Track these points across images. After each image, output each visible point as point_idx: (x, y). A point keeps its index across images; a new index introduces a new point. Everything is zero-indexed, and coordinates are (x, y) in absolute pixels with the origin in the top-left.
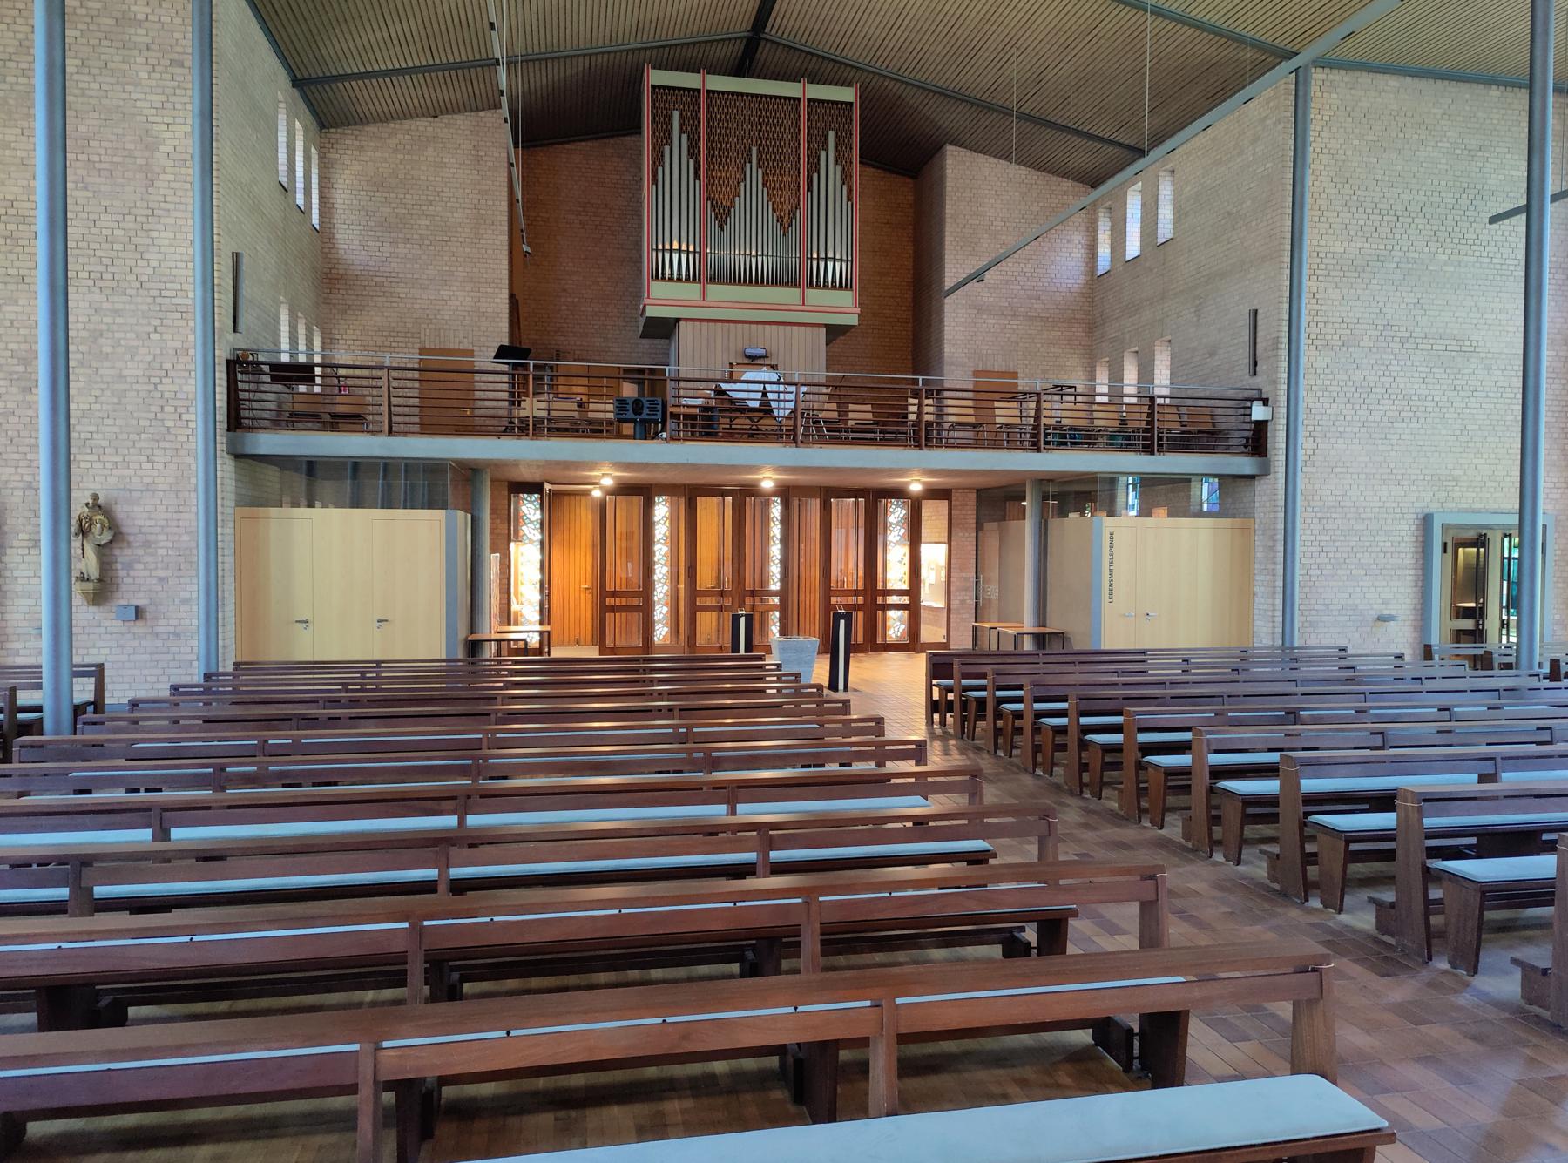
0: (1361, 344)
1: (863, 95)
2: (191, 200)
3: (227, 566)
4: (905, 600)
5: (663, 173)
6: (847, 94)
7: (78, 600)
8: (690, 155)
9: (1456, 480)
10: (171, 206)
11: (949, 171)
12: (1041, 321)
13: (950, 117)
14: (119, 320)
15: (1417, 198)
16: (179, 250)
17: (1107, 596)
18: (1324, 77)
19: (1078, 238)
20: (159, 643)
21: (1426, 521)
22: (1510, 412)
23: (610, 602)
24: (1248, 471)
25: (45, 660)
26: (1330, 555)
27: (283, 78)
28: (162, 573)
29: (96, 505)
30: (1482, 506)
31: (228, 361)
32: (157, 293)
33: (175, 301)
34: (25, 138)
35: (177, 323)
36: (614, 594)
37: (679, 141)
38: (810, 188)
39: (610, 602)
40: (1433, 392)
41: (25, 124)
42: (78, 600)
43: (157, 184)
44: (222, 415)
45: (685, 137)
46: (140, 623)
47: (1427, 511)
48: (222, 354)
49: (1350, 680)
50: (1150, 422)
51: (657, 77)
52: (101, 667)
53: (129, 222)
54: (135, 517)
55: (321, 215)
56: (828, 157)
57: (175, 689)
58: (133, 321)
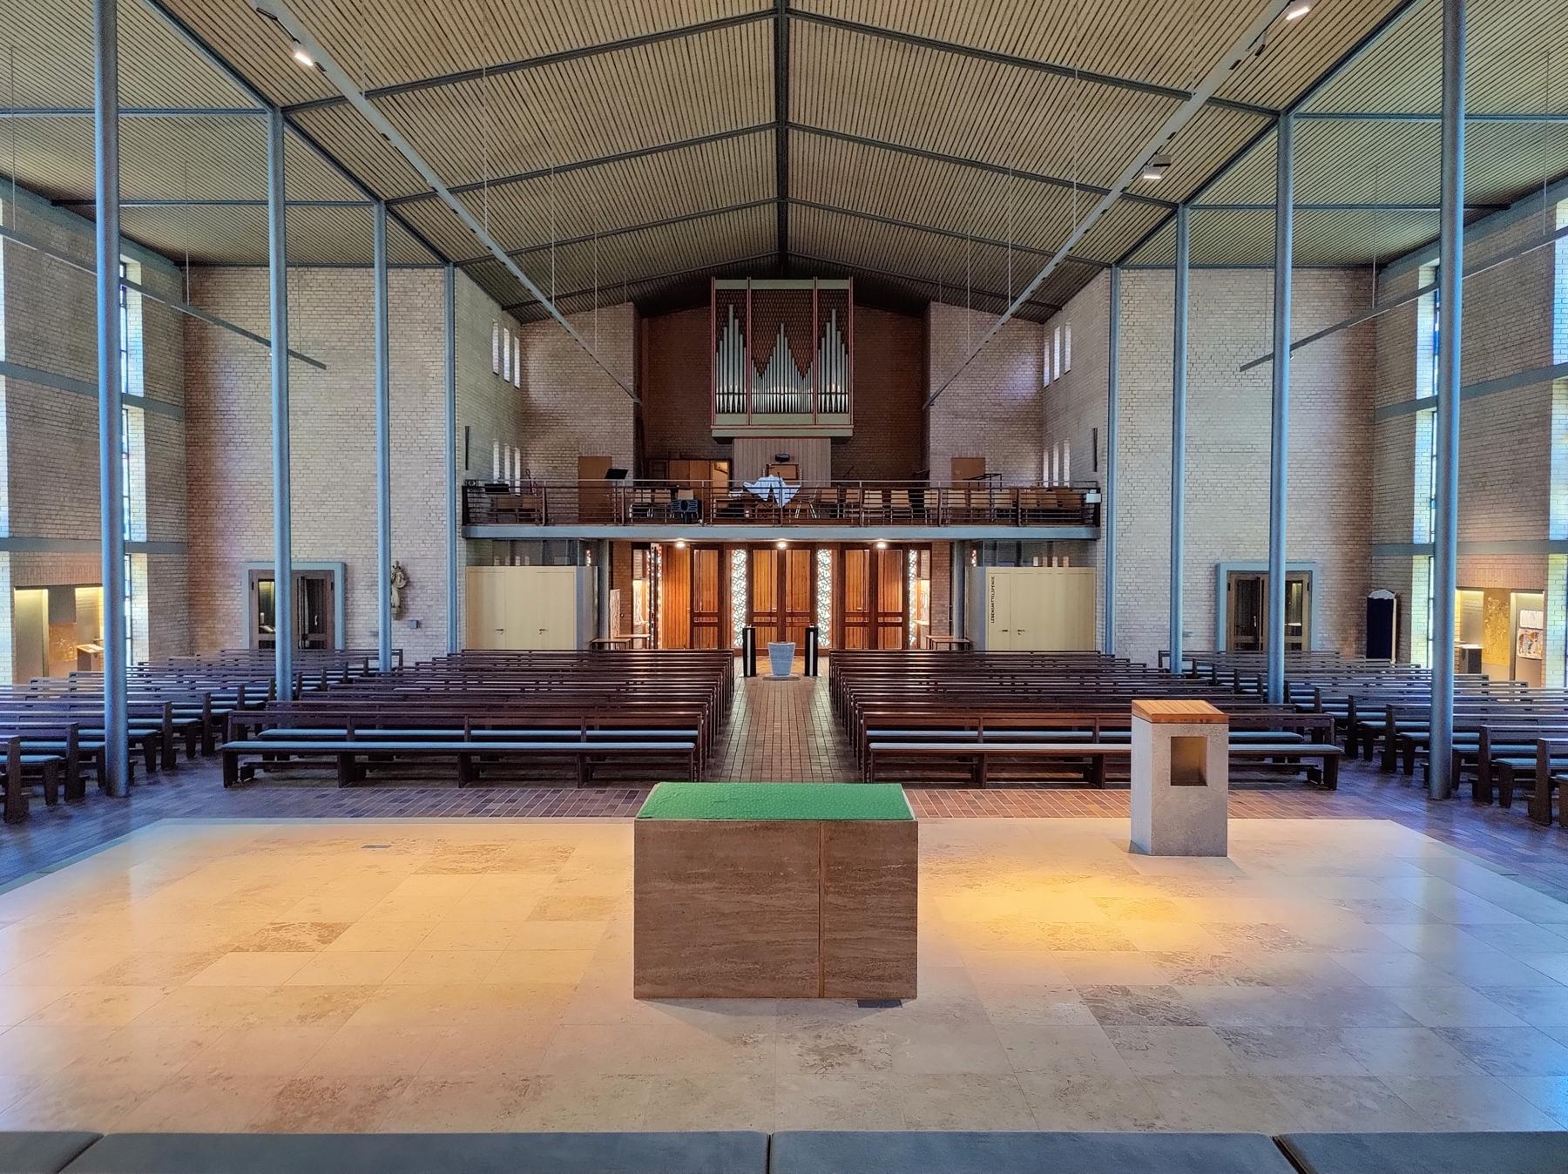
1: (856, 286)
5: (723, 345)
11: (932, 320)
18: (1135, 275)
19: (1030, 360)
21: (1217, 568)
25: (380, 647)
27: (496, 308)
36: (700, 615)
37: (733, 323)
38: (820, 348)
39: (900, 620)
44: (459, 517)
45: (737, 321)
46: (419, 630)
47: (1218, 562)
48: (460, 484)
49: (1528, 710)
50: (1016, 504)
54: (417, 572)
56: (831, 328)
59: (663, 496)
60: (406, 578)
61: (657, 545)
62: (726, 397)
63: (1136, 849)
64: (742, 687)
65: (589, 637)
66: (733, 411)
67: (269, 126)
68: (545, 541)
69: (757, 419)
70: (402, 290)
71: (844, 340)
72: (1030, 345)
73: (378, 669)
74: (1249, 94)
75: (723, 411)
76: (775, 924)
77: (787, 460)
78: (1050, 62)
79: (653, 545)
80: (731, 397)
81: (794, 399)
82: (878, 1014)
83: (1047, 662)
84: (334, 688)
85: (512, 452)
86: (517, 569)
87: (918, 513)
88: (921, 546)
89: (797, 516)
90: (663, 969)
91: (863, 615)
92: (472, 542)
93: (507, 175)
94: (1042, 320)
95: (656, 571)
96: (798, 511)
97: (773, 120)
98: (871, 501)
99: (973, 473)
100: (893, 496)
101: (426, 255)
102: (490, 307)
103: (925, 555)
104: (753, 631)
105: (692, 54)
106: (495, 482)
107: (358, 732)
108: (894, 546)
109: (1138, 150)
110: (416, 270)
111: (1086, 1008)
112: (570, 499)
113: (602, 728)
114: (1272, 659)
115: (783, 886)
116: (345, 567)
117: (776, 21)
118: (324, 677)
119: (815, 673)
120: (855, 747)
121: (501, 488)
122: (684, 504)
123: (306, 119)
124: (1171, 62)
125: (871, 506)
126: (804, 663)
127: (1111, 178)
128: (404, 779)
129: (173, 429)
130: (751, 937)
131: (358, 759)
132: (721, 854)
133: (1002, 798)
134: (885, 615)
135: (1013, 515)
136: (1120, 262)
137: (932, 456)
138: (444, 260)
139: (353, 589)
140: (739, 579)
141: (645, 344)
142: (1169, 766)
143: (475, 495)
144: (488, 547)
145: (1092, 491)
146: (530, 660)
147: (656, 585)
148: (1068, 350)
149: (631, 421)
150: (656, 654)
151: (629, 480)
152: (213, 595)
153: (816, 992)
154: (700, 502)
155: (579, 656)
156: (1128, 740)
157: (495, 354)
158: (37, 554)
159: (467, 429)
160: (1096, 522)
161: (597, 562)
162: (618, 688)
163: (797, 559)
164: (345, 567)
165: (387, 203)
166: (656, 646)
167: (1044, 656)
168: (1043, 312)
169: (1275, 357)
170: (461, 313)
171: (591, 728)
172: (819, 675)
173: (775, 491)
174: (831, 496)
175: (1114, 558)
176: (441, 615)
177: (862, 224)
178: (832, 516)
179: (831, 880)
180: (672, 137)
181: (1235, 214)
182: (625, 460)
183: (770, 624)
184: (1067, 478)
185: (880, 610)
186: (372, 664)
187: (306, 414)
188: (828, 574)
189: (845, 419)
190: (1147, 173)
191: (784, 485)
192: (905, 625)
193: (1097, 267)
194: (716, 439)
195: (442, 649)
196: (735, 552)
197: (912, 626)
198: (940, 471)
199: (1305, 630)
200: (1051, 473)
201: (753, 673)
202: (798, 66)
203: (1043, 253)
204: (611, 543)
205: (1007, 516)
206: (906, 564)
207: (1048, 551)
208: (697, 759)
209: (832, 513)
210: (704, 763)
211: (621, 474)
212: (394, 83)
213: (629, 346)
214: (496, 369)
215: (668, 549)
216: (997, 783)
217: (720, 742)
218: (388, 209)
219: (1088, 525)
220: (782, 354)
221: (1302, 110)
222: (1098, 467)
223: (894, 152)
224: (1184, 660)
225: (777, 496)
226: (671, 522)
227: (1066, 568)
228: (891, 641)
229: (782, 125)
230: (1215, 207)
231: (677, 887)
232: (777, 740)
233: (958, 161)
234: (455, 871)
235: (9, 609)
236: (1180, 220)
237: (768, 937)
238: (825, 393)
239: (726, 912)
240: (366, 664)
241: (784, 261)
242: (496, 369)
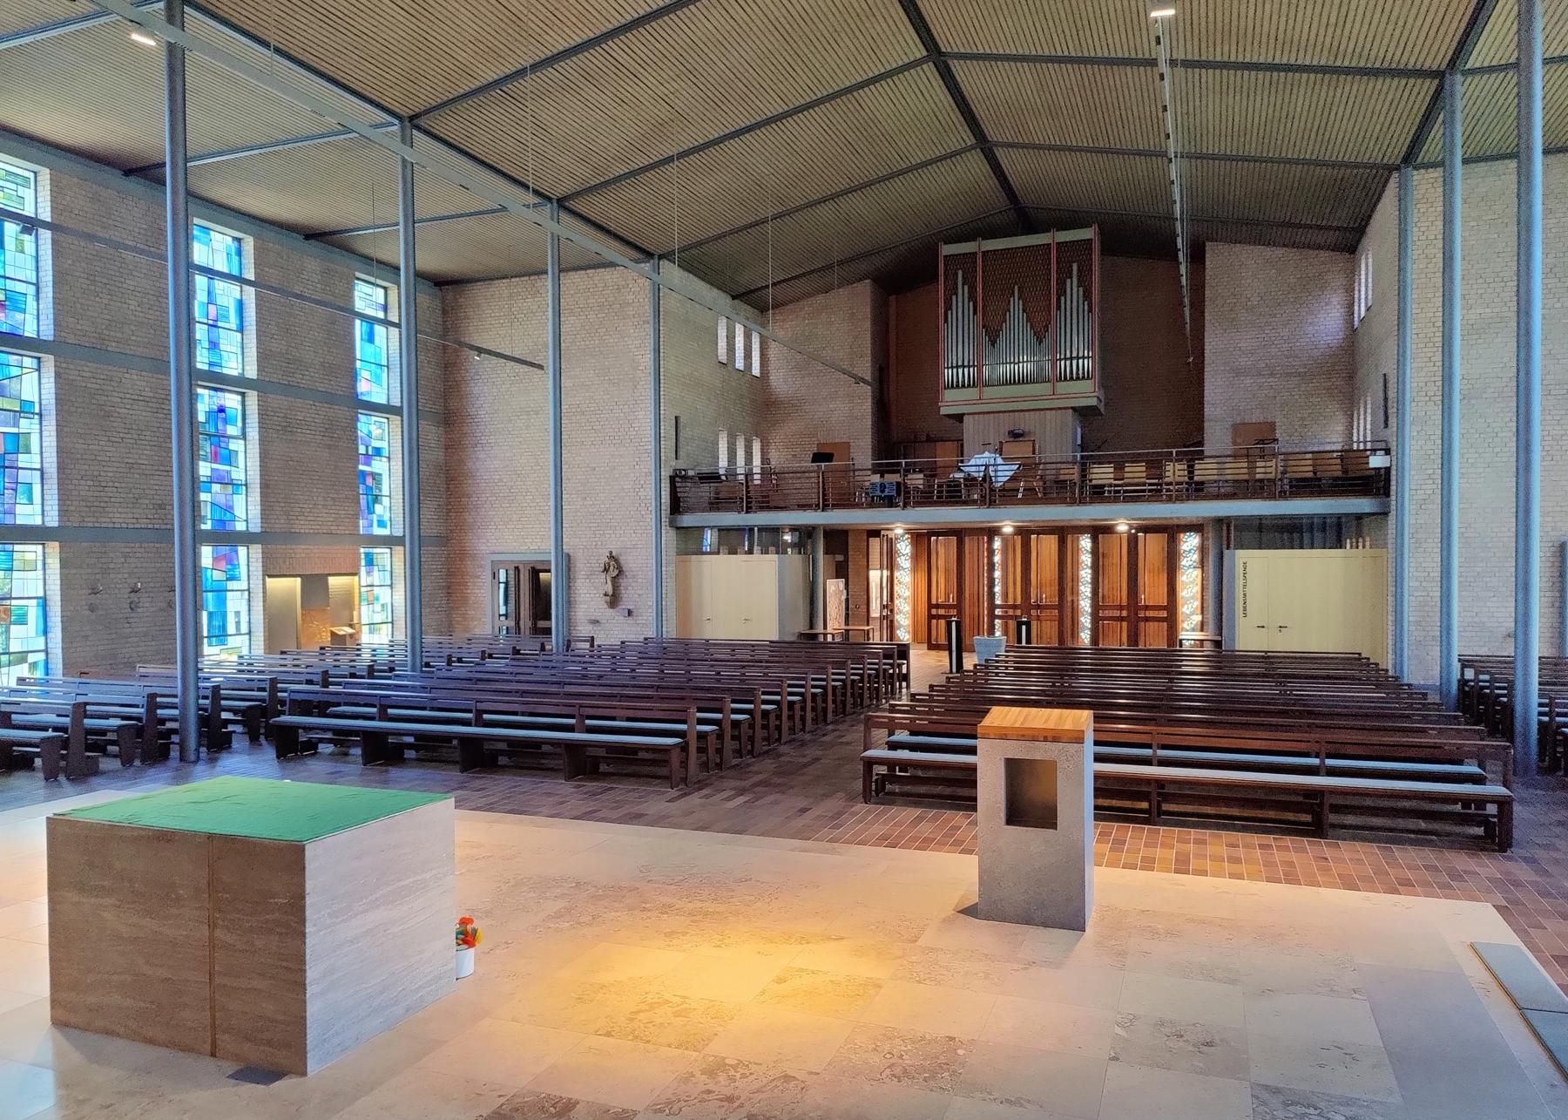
0: (1484, 396)
1: (1103, 233)
4: (1164, 614)
5: (952, 316)
6: (1087, 234)
12: (1299, 376)
23: (934, 612)
27: (728, 300)
28: (639, 592)
29: (611, 557)
36: (938, 606)
37: (963, 291)
38: (1059, 308)
39: (934, 612)
45: (966, 287)
47: (1563, 539)
48: (666, 473)
51: (947, 250)
54: (628, 563)
55: (762, 365)
56: (1073, 285)
62: (955, 370)
69: (989, 392)
71: (1087, 296)
72: (1338, 281)
77: (1021, 435)
79: (882, 532)
80: (960, 371)
87: (1196, 490)
88: (1196, 527)
92: (683, 531)
99: (1258, 440)
112: (808, 487)
113: (629, 719)
123: (422, 122)
129: (432, 434)
131: (591, 752)
134: (1147, 608)
138: (649, 255)
139: (574, 578)
145: (1378, 453)
152: (465, 584)
155: (778, 649)
156: (972, 751)
158: (289, 547)
168: (1349, 241)
191: (1000, 461)
198: (1217, 438)
209: (1058, 491)
213: (866, 326)
225: (992, 474)
228: (1154, 638)
235: (261, 595)
241: (1024, 218)
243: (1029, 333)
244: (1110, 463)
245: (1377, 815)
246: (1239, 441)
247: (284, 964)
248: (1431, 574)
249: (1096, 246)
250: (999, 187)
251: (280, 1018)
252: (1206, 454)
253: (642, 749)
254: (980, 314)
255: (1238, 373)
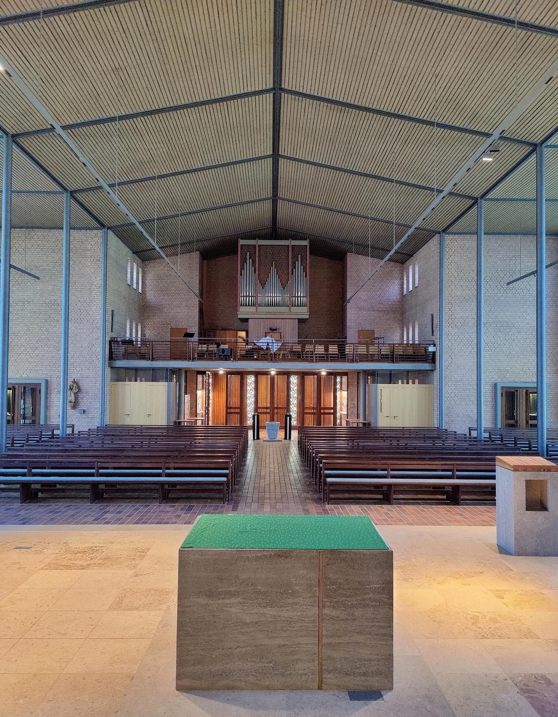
2: (101, 297)
3: (107, 399)
7: (69, 408)
8: (253, 265)
9: (508, 371)
10: (96, 299)
11: (348, 261)
13: (345, 246)
14: (82, 331)
15: (489, 275)
16: (98, 311)
17: (380, 410)
18: (452, 237)
19: (397, 282)
20: (89, 420)
21: (496, 385)
22: (528, 347)
24: (428, 368)
25: (61, 424)
26: (458, 397)
27: (130, 253)
28: (91, 401)
29: (74, 382)
30: (518, 380)
31: (109, 341)
32: (91, 323)
33: (96, 325)
34: (59, 283)
35: (96, 331)
36: (231, 408)
37: (249, 261)
38: (292, 274)
39: (332, 411)
40: (497, 341)
41: (60, 279)
42: (69, 408)
43: (92, 293)
45: (251, 260)
47: (496, 382)
48: (108, 339)
52: (74, 425)
53: (85, 304)
54: (84, 385)
56: (298, 264)
57: (89, 430)
58: (85, 331)
59: (213, 347)
60: (79, 387)
61: (209, 373)
62: (245, 298)
63: (503, 550)
64: (252, 445)
65: (174, 418)
66: (249, 305)
67: (4, 145)
68: (153, 369)
69: (261, 309)
70: (81, 240)
71: (305, 270)
72: (396, 274)
73: (59, 435)
74: (521, 134)
75: (244, 305)
76: (285, 631)
77: (276, 330)
78: (418, 117)
79: (207, 372)
81: (279, 299)
82: (366, 708)
83: (412, 433)
84: (45, 441)
85: (137, 325)
86: (138, 383)
87: (342, 356)
89: (281, 357)
90: (199, 667)
91: (314, 408)
93: (134, 179)
94: (403, 263)
95: (209, 386)
96: (281, 355)
97: (271, 153)
98: (319, 350)
100: (330, 347)
101: (95, 223)
102: (125, 250)
103: (345, 379)
104: (258, 416)
105: (230, 112)
106: (127, 339)
107: (33, 470)
108: (329, 374)
109: (460, 167)
110: (88, 231)
111: (523, 698)
112: (165, 348)
113: (175, 469)
114: (540, 433)
115: (291, 601)
116: (47, 381)
117: (274, 94)
118: (41, 436)
119: (290, 438)
120: (316, 478)
121: (130, 342)
122: (223, 350)
123: (24, 142)
124: (482, 116)
125: (319, 352)
126: (284, 433)
127: (444, 184)
128: (60, 498)
130: (266, 642)
131: (33, 486)
132: (244, 576)
133: (404, 511)
134: (325, 408)
135: (391, 358)
136: (444, 231)
137: (348, 329)
138: (103, 226)
140: (251, 390)
141: (205, 273)
142: (524, 498)
143: (116, 345)
144: (123, 371)
145: (431, 345)
146: (141, 431)
147: (209, 393)
148: (417, 276)
149: (197, 310)
150: (208, 427)
151: (196, 338)
153: (316, 685)
154: (231, 349)
155: (168, 428)
156: (494, 478)
157: (129, 275)
159: (113, 311)
160: (433, 361)
161: (178, 380)
162: (186, 446)
163: (280, 381)
164: (47, 381)
165: (71, 192)
166: (208, 424)
167: (411, 429)
169: (536, 273)
170: (111, 253)
171: (169, 469)
172: (292, 439)
173: (270, 344)
174: (298, 348)
175: (443, 380)
176: (97, 407)
177: (316, 211)
178: (298, 357)
179: (327, 597)
180: (219, 161)
181: (507, 203)
182: (195, 329)
183: (266, 413)
184: (417, 338)
185: (322, 406)
186: (56, 432)
187: (29, 303)
188: (296, 388)
189: (305, 310)
190: (484, 157)
192: (335, 414)
193: (434, 233)
194: (240, 319)
195: (95, 424)
196: (249, 377)
197: (338, 414)
198: (352, 335)
199: (539, 418)
200: (408, 337)
201: (258, 438)
202: (285, 122)
203: (384, 250)
204: (186, 372)
205: (388, 358)
206: (335, 383)
207: (407, 376)
208: (228, 486)
209: (298, 356)
210: (232, 489)
211: (192, 335)
212: (72, 123)
214: (129, 282)
215: (215, 375)
216: (399, 502)
217: (241, 476)
218: (71, 195)
219: (429, 362)
220: (273, 277)
221: (487, 198)
222: (434, 333)
223: (333, 170)
224: (484, 432)
225: (270, 347)
226: (216, 360)
227: (417, 385)
229: (276, 156)
230: (497, 200)
231: (210, 602)
232: (272, 475)
233: (366, 175)
234: (68, 567)
236: (479, 206)
237: (278, 641)
238: (295, 297)
239: (248, 621)
240: (53, 433)
242: (129, 282)
243: (280, 284)
244: (323, 344)
245: (365, 494)
246: (361, 337)
247: (377, 624)
248: (451, 395)
249: (308, 248)
250: (271, 218)
251: (372, 657)
252: (348, 342)
253: (447, 486)
254: (257, 272)
255: (360, 309)
